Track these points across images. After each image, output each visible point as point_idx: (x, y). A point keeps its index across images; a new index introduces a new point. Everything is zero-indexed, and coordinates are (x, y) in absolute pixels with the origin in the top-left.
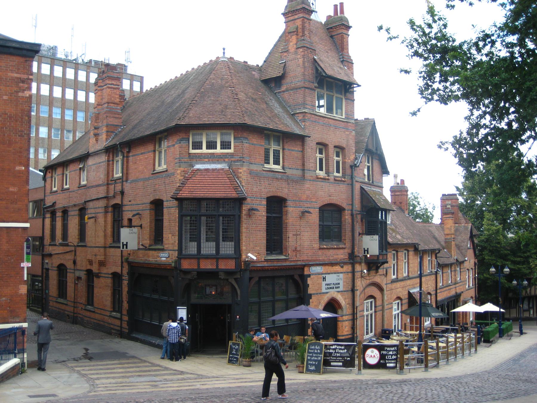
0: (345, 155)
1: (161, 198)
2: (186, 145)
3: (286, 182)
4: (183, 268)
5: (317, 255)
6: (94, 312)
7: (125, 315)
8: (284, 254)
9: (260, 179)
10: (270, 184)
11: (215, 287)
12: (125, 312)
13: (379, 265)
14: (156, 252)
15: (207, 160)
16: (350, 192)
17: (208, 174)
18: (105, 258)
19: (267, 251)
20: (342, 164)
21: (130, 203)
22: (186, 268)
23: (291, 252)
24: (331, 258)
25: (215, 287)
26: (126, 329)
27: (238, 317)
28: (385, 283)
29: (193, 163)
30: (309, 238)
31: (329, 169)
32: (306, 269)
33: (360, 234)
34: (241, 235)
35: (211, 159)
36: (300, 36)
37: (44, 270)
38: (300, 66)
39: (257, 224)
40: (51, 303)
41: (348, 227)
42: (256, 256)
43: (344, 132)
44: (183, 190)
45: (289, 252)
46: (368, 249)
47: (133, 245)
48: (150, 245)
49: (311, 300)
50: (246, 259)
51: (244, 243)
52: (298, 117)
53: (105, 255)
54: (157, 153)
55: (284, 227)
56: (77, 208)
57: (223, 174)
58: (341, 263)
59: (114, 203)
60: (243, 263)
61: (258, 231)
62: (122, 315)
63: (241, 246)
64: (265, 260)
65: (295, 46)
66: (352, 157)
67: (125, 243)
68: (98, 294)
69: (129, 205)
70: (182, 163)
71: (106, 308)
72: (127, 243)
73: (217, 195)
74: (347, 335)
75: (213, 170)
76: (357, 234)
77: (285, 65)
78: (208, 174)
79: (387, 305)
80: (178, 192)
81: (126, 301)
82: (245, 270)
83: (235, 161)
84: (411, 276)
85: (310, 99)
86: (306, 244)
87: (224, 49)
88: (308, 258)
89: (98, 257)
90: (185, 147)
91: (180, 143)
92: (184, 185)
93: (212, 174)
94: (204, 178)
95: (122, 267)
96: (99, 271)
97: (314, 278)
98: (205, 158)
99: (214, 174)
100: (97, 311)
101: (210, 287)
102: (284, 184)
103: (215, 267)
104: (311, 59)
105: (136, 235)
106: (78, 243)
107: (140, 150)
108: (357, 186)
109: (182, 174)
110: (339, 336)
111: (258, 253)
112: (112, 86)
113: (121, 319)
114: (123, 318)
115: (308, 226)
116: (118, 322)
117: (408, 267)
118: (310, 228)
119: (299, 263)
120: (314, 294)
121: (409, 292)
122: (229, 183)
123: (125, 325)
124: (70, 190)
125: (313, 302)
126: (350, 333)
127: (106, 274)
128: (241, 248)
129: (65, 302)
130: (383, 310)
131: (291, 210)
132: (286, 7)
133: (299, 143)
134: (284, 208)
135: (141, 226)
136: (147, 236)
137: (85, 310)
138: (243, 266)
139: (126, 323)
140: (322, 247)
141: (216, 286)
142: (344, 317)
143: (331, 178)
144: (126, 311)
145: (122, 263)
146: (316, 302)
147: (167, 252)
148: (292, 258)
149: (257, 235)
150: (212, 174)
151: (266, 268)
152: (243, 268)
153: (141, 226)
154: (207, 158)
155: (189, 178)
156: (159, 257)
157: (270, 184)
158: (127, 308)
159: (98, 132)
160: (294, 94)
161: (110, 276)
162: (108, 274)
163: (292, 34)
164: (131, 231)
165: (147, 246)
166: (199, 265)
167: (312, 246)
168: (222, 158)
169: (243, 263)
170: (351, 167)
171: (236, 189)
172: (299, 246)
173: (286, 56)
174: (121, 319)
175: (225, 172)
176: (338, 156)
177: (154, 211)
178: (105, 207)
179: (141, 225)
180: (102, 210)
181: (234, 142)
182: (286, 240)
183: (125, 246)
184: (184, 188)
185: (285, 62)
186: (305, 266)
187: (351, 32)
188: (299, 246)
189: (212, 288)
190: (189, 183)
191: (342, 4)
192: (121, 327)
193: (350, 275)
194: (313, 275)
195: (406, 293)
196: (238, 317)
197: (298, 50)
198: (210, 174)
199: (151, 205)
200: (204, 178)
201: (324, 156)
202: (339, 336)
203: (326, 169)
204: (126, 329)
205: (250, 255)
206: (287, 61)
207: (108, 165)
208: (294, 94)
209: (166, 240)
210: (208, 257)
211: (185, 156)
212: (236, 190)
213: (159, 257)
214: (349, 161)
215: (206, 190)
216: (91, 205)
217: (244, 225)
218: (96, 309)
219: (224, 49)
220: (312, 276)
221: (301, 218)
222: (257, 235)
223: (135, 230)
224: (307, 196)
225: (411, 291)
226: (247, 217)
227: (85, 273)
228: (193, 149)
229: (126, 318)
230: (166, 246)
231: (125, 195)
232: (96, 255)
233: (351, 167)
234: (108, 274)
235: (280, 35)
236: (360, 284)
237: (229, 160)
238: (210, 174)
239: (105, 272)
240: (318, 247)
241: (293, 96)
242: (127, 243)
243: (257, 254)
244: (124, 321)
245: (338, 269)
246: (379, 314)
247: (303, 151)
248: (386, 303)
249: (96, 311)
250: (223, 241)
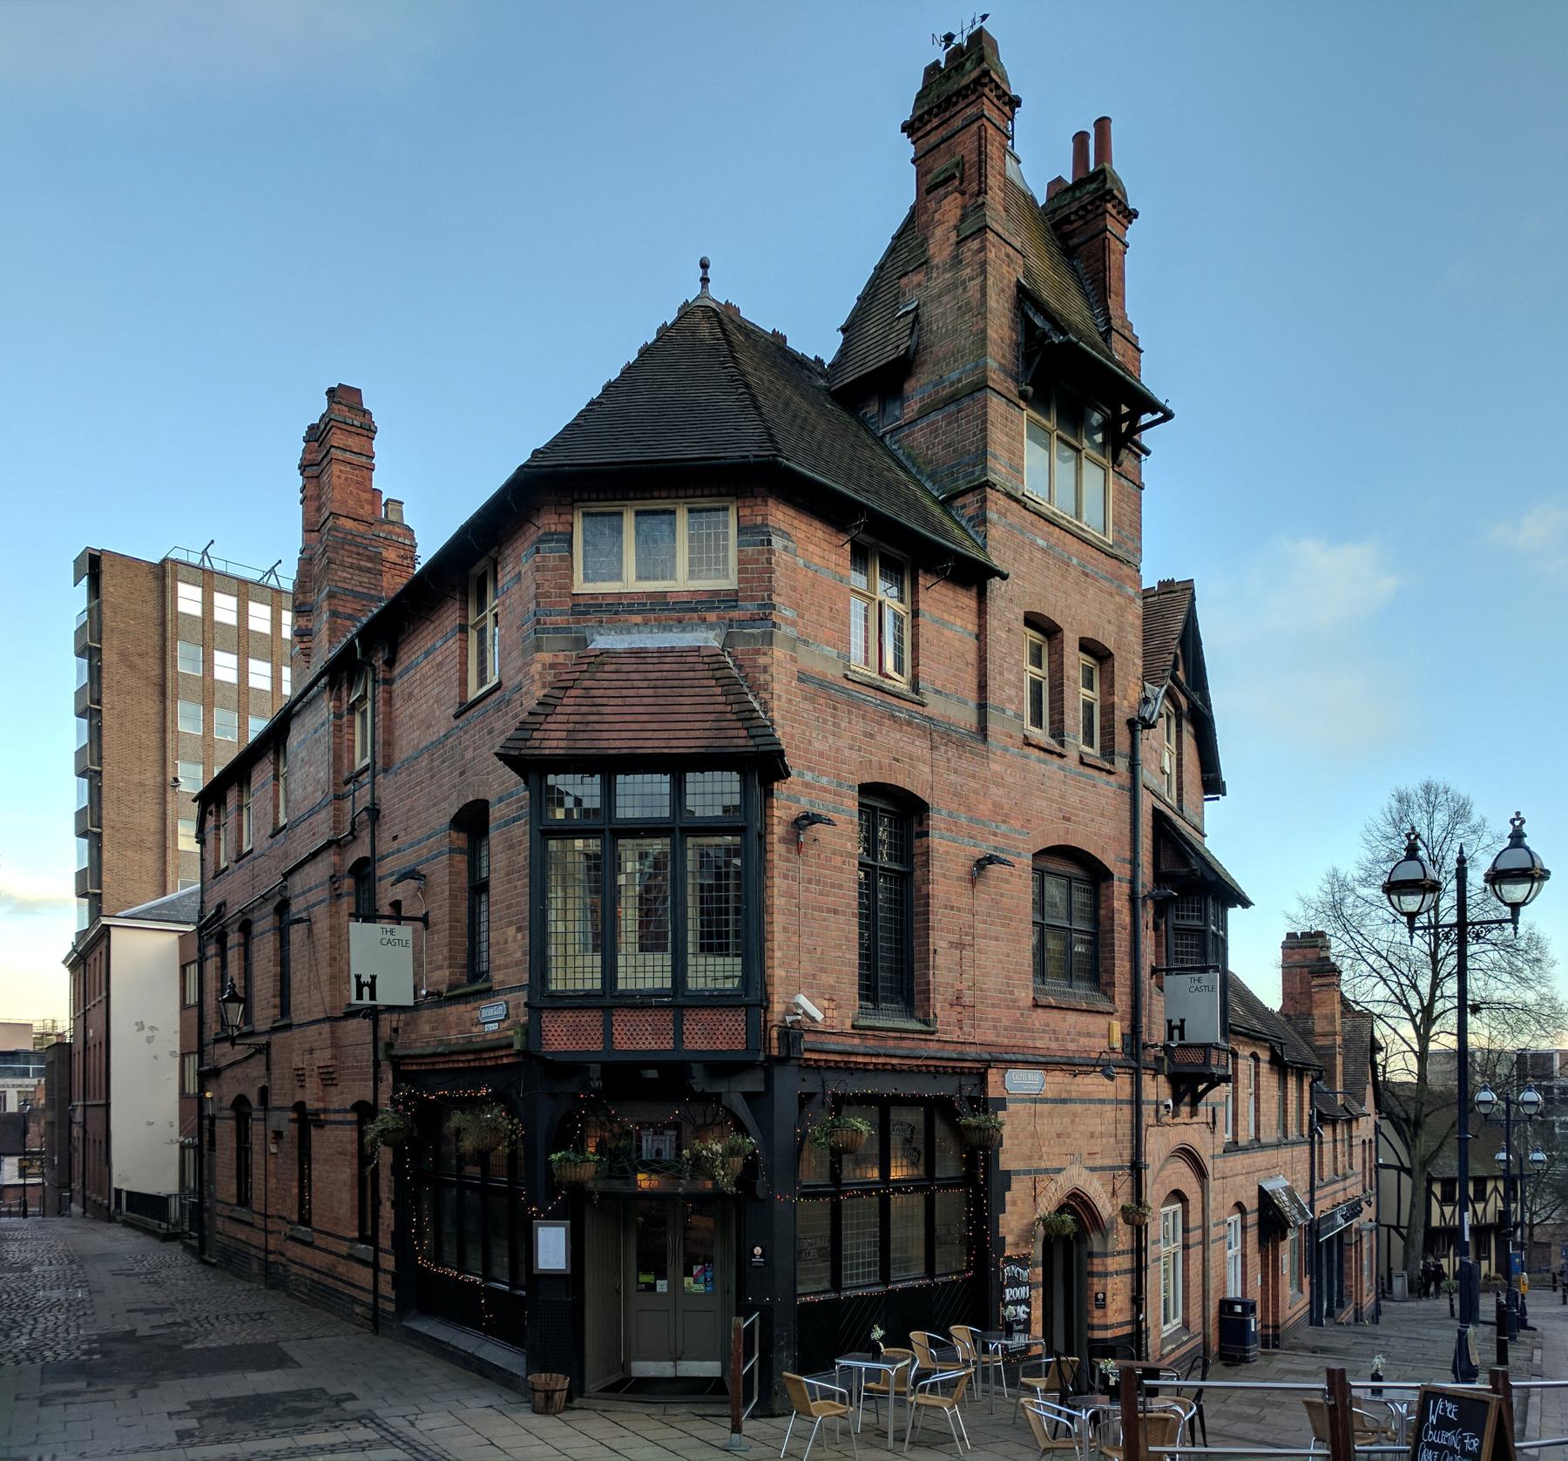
0: (1113, 680)
1: (481, 797)
2: (562, 559)
3: (925, 737)
4: (546, 1049)
5: (1029, 1030)
6: (310, 1244)
7: (386, 1251)
8: (918, 1013)
9: (835, 708)
10: (871, 736)
11: (674, 1133)
12: (385, 1241)
13: (1201, 1088)
14: (469, 1007)
15: (638, 619)
16: (1126, 816)
17: (642, 667)
18: (334, 1057)
19: (861, 997)
20: (1102, 715)
21: (395, 845)
22: (561, 1048)
23: (942, 1009)
24: (1071, 1046)
25: (674, 1133)
26: (390, 1300)
27: (758, 1250)
28: (1211, 1152)
29: (588, 632)
30: (1000, 961)
31: (1062, 720)
32: (993, 1076)
33: (1154, 971)
34: (767, 918)
35: (652, 616)
36: (972, 195)
37: (206, 1122)
38: (971, 309)
39: (825, 884)
40: (220, 1224)
41: (1120, 939)
42: (824, 1010)
43: (1111, 594)
44: (544, 727)
45: (938, 1005)
46: (1182, 1021)
47: (396, 989)
48: (451, 987)
49: (1008, 1194)
50: (789, 1019)
51: (778, 954)
52: (963, 507)
53: (335, 1044)
54: (473, 636)
55: (918, 914)
56: (270, 907)
57: (701, 666)
58: (1104, 1067)
59: (355, 858)
60: (774, 1034)
61: (829, 910)
62: (377, 1250)
63: (768, 963)
64: (853, 1027)
65: (953, 238)
66: (1134, 694)
67: (366, 979)
68: (321, 1184)
69: (393, 854)
70: (544, 631)
71: (341, 1231)
72: (374, 978)
73: (675, 743)
74: (1120, 1325)
75: (662, 652)
76: (1145, 972)
77: (917, 317)
78: (642, 667)
79: (1215, 1225)
80: (526, 735)
81: (388, 1199)
82: (783, 1061)
83: (742, 623)
84: (1264, 1140)
85: (1005, 439)
86: (993, 983)
87: (704, 265)
88: (998, 1036)
89: (317, 1054)
90: (556, 568)
91: (538, 551)
92: (549, 710)
93: (657, 667)
94: (628, 684)
95: (377, 1079)
96: (321, 1105)
97: (1018, 1112)
98: (631, 612)
99: (666, 667)
100: (320, 1241)
101: (655, 1133)
102: (920, 747)
103: (670, 1046)
104: (1009, 287)
105: (408, 953)
106: (275, 1022)
107: (422, 643)
108: (1146, 803)
109: (549, 679)
110: (1092, 1327)
111: (831, 1000)
112: (348, 455)
113: (375, 1266)
114: (381, 1261)
115: (999, 917)
116: (364, 1276)
117: (1257, 1110)
118: (1003, 925)
119: (972, 1052)
120: (1018, 1173)
121: (1260, 1188)
122: (722, 699)
123: (386, 1288)
124: (255, 853)
125: (1014, 1203)
126: (1127, 1317)
127: (338, 1111)
128: (768, 972)
129: (248, 1219)
130: (1204, 1243)
131: (941, 850)
132: (920, 97)
133: (968, 600)
134: (917, 842)
135: (425, 919)
136: (442, 954)
137: (292, 1238)
138: (775, 1043)
139: (389, 1277)
140: (1043, 1001)
141: (676, 1126)
142: (1109, 1260)
143: (1072, 755)
144: (389, 1237)
145: (377, 1064)
146: (1023, 1202)
147: (501, 1000)
148: (945, 1032)
149: (826, 928)
150: (657, 667)
151: (860, 1059)
152: (775, 1052)
153: (425, 919)
154: (639, 612)
155: (571, 684)
156: (478, 1023)
157: (871, 736)
158: (392, 1228)
159: (310, 625)
160: (949, 424)
161: (352, 1117)
162: (345, 1111)
163: (942, 191)
164: (389, 936)
165: (443, 988)
166: (608, 1035)
167: (1011, 993)
168: (695, 610)
169: (774, 1034)
170: (1131, 724)
171: (747, 717)
172: (969, 988)
173: (919, 285)
174: (375, 1266)
175: (706, 660)
176: (1089, 685)
177: (466, 857)
178: (331, 877)
179: (427, 914)
180: (323, 893)
181: (740, 544)
182: (926, 960)
183: (366, 990)
184: (550, 719)
185: (917, 308)
186: (988, 1064)
187: (1133, 233)
188: (969, 988)
189: (662, 1134)
190: (571, 701)
191: (1102, 124)
192: (375, 1292)
193: (1126, 1112)
194: (1015, 1101)
195: (1254, 1192)
196: (758, 1250)
197: (965, 249)
198: (651, 667)
199: (454, 835)
200: (628, 684)
201: (1044, 672)
202: (1092, 1327)
203: (1051, 723)
204: (390, 1300)
205: (802, 999)
206: (924, 305)
207: (338, 729)
208: (949, 424)
209: (500, 951)
210: (640, 1002)
211: (555, 603)
212: (747, 724)
213: (478, 1023)
214: (1126, 703)
215: (634, 726)
216: (298, 881)
217: (777, 881)
218: (315, 1234)
219: (704, 265)
220: (1011, 1107)
221: (973, 882)
222: (826, 928)
223: (405, 931)
224: (995, 804)
225: (1268, 1187)
226: (789, 851)
227: (294, 1115)
228: (586, 579)
229: (388, 1262)
230: (498, 977)
231: (382, 821)
232: (311, 1051)
233: (1131, 724)
234: (345, 1111)
235: (894, 232)
236: (1158, 1143)
237: (719, 618)
238: (651, 667)
239: (336, 1106)
240: (1030, 1002)
241: (944, 433)
242: (374, 978)
243: (826, 1004)
244: (385, 1271)
245: (1091, 1088)
246: (1195, 1253)
247: (982, 612)
248: (1212, 1220)
249: (317, 1243)
250: (706, 948)
